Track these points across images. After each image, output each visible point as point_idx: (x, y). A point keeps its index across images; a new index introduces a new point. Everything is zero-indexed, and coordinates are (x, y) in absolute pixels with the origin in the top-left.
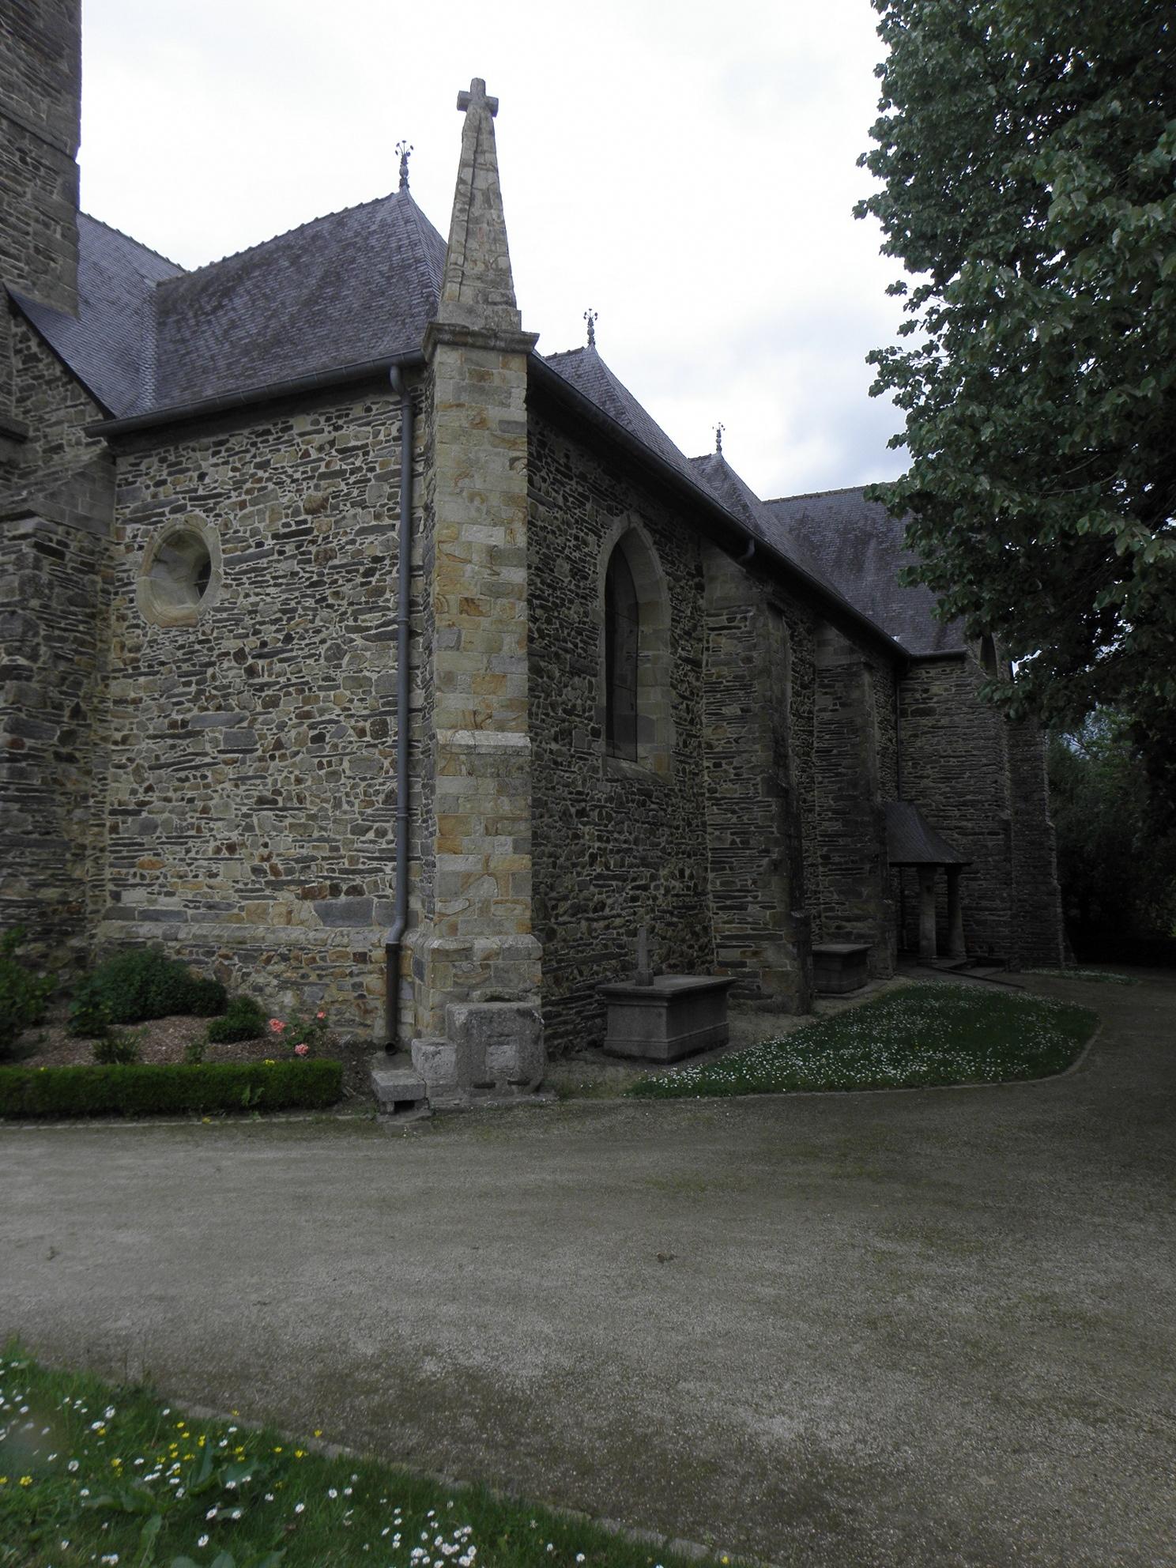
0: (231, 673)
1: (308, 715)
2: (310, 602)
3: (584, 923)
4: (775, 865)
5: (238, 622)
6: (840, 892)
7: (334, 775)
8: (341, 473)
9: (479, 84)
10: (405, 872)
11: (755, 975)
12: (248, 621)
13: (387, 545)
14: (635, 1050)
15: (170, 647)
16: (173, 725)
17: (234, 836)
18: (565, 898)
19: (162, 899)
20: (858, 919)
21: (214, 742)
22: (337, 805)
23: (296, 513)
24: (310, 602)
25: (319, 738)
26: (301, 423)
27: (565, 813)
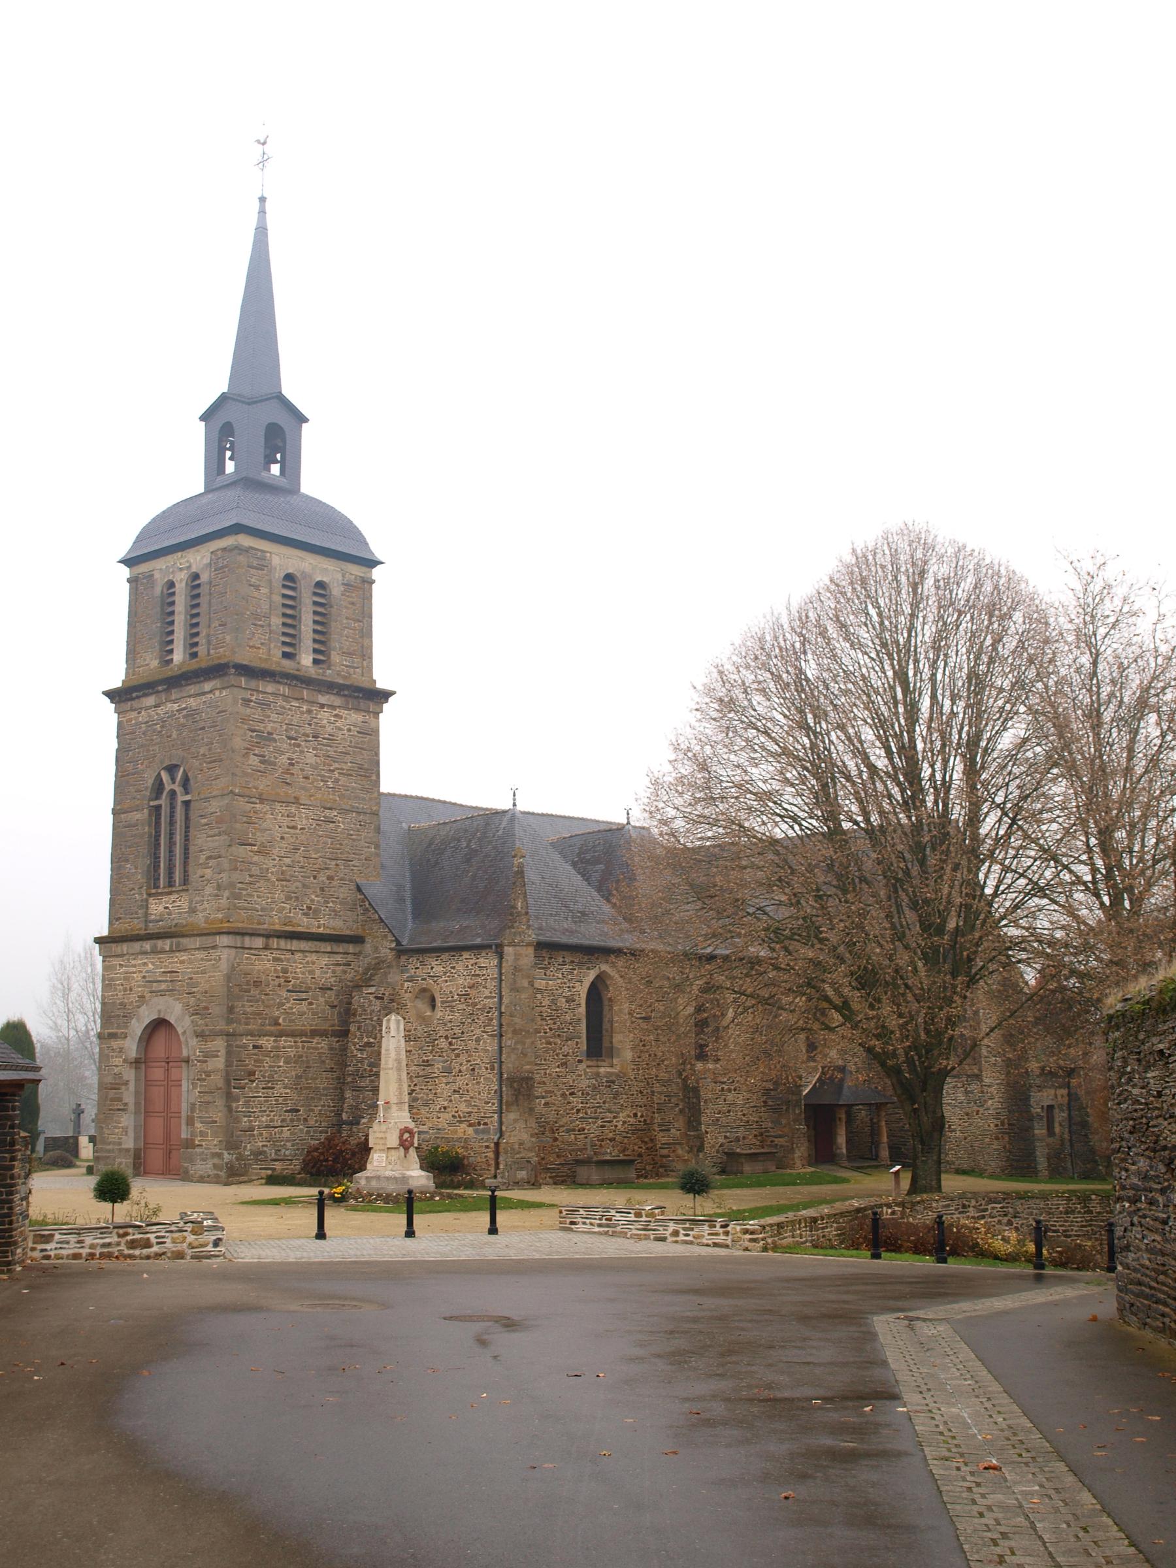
0: (443, 1043)
1: (469, 1061)
2: (469, 1021)
3: (573, 1136)
4: (681, 1111)
5: (446, 1025)
6: (772, 1122)
7: (478, 1083)
8: (478, 975)
10: (500, 1117)
11: (673, 1161)
12: (449, 1025)
13: (493, 1003)
14: (584, 1182)
15: (422, 1032)
16: (423, 1061)
17: (446, 1104)
18: (563, 1126)
19: (421, 1127)
20: (780, 1136)
21: (438, 1069)
22: (479, 1094)
23: (464, 987)
24: (469, 1021)
25: (473, 1070)
26: (466, 955)
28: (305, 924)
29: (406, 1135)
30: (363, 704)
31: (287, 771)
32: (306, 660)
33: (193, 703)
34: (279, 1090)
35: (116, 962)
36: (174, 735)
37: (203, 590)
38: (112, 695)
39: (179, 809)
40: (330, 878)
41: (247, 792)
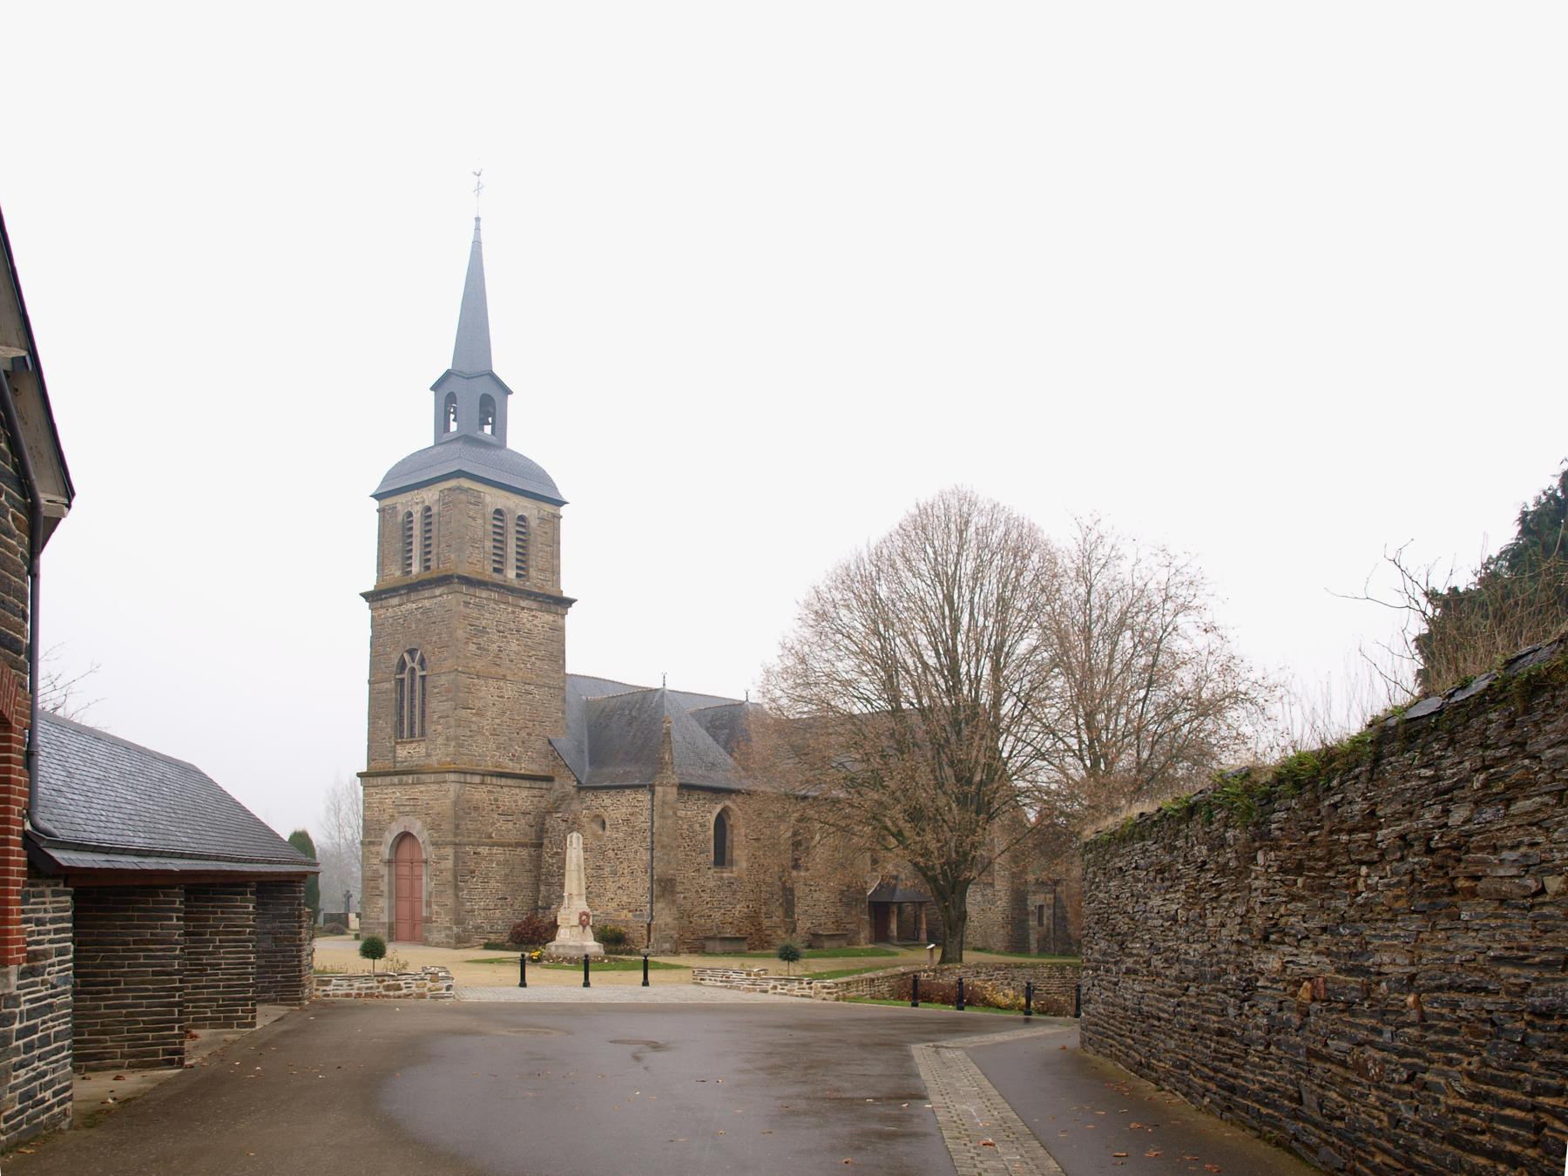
0: (611, 854)
9: (363, 595)
10: (652, 907)
26: (628, 792)
27: (697, 891)
28: (511, 767)
29: (584, 917)
30: (553, 608)
31: (497, 656)
32: (511, 574)
33: (427, 603)
34: (493, 884)
35: (373, 790)
36: (414, 627)
37: (434, 520)
38: (366, 596)
39: (418, 681)
40: (529, 734)
41: (467, 670)
